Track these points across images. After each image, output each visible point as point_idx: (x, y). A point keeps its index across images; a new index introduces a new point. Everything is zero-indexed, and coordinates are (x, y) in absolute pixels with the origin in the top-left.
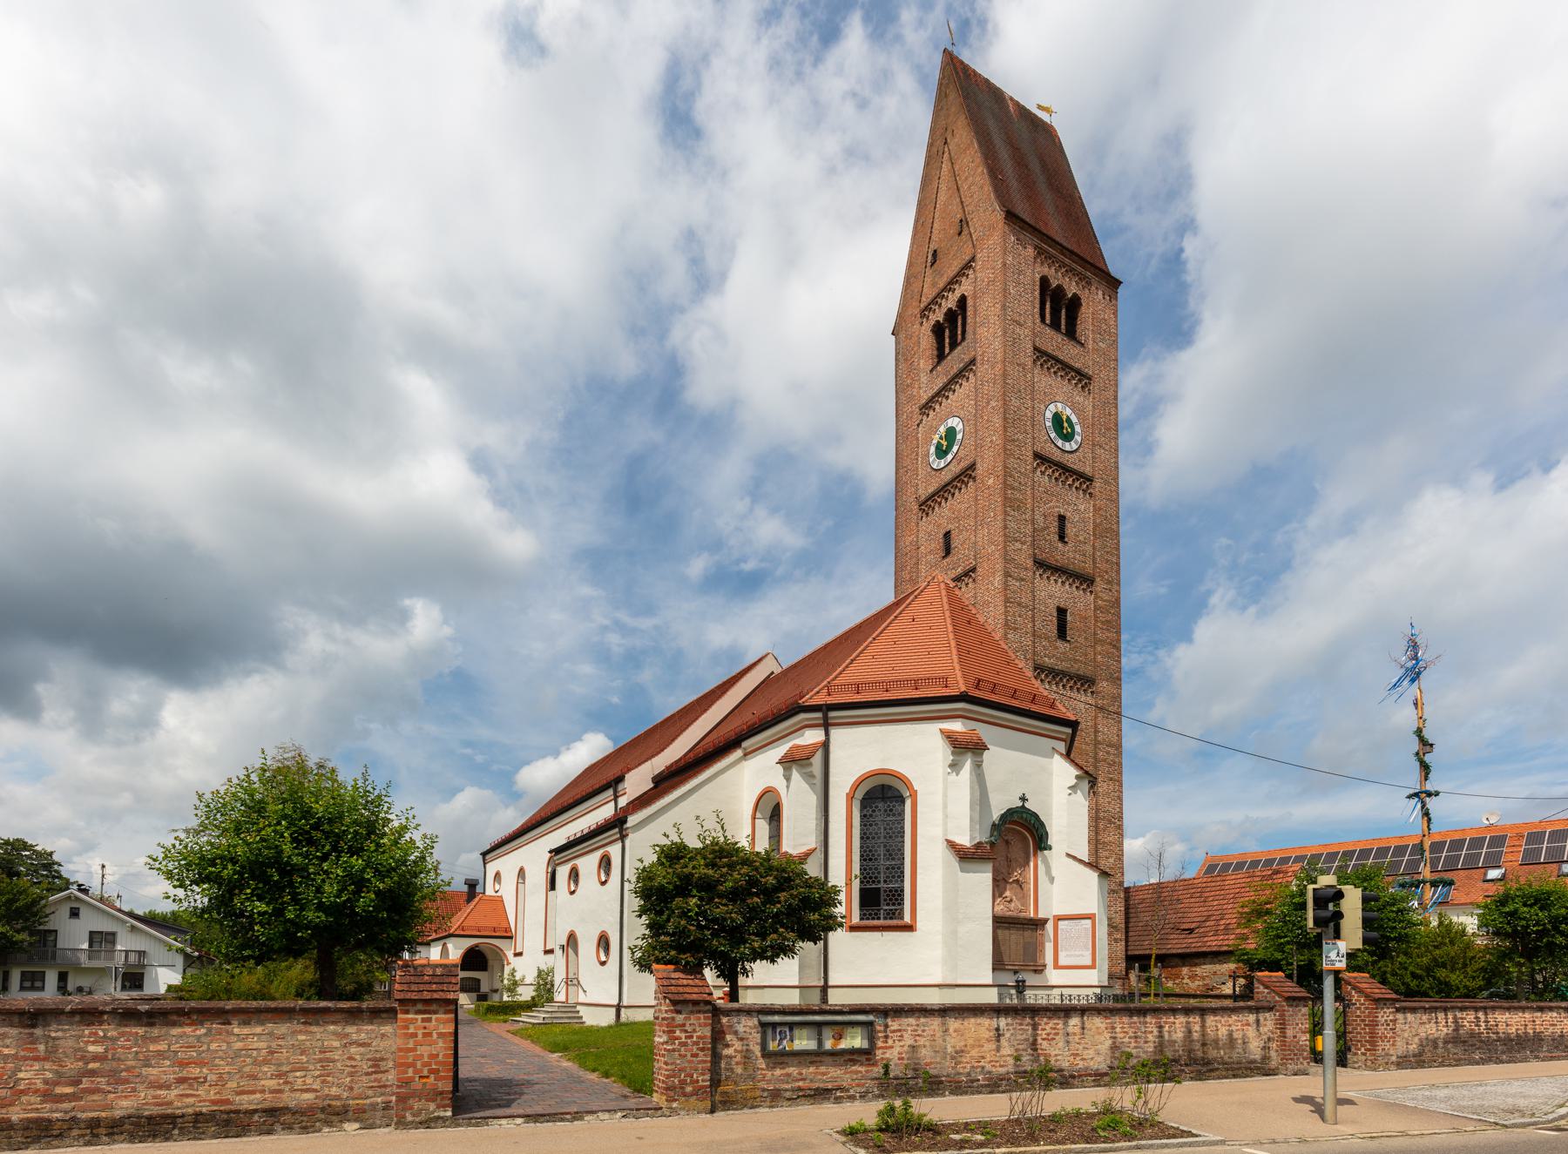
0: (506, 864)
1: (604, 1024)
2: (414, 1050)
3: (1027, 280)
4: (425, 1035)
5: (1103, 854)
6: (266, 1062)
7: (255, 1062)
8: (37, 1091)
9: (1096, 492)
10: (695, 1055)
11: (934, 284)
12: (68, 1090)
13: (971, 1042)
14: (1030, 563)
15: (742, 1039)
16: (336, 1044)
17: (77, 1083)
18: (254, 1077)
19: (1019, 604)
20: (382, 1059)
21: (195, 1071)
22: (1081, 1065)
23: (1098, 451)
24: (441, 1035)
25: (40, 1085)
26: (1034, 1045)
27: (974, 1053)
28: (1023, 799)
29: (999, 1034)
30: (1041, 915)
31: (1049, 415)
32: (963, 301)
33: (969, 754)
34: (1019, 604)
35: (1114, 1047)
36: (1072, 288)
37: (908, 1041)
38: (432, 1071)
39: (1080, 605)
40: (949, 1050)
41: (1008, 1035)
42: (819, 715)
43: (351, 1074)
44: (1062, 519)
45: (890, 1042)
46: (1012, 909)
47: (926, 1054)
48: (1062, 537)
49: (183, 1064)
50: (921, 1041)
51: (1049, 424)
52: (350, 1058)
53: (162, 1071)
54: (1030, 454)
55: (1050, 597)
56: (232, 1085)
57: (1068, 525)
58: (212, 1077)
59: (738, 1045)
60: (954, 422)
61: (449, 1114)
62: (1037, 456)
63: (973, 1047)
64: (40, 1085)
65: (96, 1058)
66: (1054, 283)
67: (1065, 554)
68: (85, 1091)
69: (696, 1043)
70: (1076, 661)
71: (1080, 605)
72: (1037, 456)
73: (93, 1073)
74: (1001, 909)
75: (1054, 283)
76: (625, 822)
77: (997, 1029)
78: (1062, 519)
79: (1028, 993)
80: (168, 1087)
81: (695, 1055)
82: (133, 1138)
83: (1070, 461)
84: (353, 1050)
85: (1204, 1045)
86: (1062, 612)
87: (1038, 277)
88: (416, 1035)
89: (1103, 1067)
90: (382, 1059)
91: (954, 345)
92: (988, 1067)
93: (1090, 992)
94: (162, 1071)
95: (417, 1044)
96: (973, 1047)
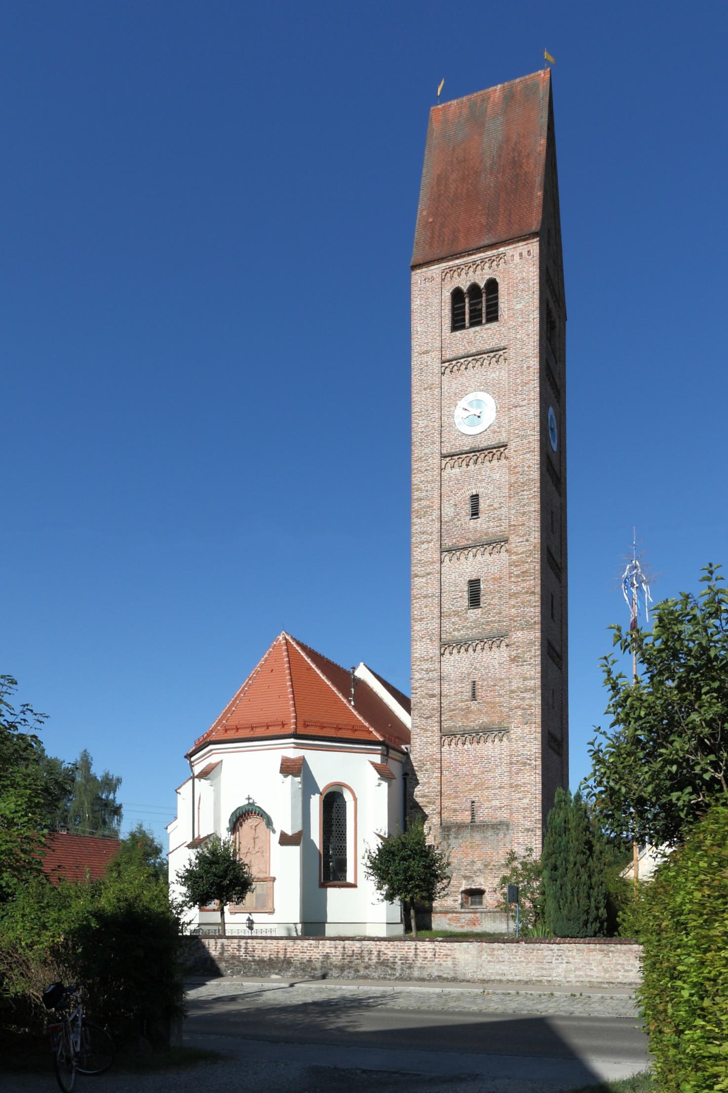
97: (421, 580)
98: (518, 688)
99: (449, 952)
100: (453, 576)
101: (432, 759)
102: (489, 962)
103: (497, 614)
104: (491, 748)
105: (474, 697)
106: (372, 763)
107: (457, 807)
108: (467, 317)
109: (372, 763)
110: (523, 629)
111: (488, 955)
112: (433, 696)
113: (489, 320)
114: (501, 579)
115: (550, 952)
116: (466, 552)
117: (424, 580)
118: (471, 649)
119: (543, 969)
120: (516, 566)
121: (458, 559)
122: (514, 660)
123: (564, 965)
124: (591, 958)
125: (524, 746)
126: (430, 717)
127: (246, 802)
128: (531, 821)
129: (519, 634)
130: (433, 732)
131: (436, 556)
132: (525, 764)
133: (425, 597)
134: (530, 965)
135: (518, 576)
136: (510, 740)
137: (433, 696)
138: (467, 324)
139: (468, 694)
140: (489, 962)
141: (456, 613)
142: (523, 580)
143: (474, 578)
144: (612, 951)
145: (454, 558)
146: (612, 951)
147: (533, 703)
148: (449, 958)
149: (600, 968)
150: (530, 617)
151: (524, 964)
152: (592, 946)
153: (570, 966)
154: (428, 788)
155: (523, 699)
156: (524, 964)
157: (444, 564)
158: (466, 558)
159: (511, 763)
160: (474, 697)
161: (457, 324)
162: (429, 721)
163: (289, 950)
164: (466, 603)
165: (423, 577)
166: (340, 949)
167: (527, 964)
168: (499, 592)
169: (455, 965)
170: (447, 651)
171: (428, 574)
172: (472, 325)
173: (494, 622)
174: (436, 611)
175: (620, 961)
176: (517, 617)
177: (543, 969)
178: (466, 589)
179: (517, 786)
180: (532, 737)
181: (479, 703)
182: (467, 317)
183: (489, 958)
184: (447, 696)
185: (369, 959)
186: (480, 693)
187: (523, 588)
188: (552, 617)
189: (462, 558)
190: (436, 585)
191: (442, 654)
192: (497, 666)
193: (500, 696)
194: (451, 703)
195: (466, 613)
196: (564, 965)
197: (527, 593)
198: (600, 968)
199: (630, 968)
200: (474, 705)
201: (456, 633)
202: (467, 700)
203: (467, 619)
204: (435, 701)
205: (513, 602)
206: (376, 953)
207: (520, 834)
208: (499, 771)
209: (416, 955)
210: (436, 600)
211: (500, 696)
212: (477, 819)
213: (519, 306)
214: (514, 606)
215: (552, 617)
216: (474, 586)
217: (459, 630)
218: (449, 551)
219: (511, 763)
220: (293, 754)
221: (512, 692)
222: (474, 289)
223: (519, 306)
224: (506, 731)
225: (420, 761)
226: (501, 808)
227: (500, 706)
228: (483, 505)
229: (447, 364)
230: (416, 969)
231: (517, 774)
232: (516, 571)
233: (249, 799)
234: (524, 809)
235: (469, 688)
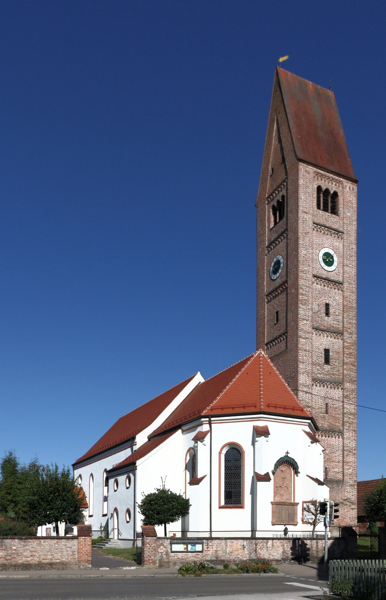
0: (84, 471)
1: (379, 477)
2: (82, 549)
3: (310, 190)
4: (85, 545)
5: (346, 467)
6: (49, 551)
7: (47, 552)
8: (3, 558)
9: (345, 289)
10: (152, 552)
11: (272, 185)
12: (9, 558)
13: (235, 549)
14: (310, 329)
15: (165, 547)
16: (64, 547)
17: (10, 556)
18: (46, 555)
19: (305, 350)
20: (74, 551)
21: (34, 553)
22: (272, 558)
23: (346, 268)
24: (88, 545)
25: (4, 556)
26: (256, 551)
27: (236, 553)
28: (287, 453)
29: (244, 547)
30: (296, 502)
31: (321, 255)
32: (283, 197)
33: (263, 437)
34: (305, 350)
35: (284, 552)
36: (333, 188)
37: (215, 549)
38: (86, 555)
39: (336, 347)
40: (228, 552)
41: (247, 547)
42: (208, 419)
43: (68, 555)
44: (327, 305)
45: (209, 549)
46: (284, 499)
47: (220, 553)
48: (327, 314)
49: (31, 552)
50: (219, 549)
51: (280, 271)
52: (67, 551)
53: (27, 553)
54: (311, 276)
55: (321, 345)
56: (42, 557)
57: (330, 308)
58: (37, 555)
59: (164, 549)
60: (280, 257)
61: (91, 566)
62: (343, 233)
63: (235, 551)
64: (4, 556)
65: (15, 550)
66: (324, 188)
67: (329, 321)
68: (13, 558)
69: (152, 548)
70: (333, 374)
71: (336, 347)
72: (314, 276)
73: (13, 553)
74: (278, 499)
75: (324, 188)
76: (135, 464)
77: (243, 545)
78: (327, 305)
79: (289, 533)
80: (29, 557)
81: (152, 552)
82: (22, 569)
83: (332, 277)
84: (68, 549)
85: (317, 552)
86: (327, 351)
87: (316, 186)
88: (82, 545)
89: (280, 558)
90: (74, 551)
91: (281, 218)
92: (240, 557)
93: (308, 533)
94: (27, 553)
95: (83, 547)
96: (235, 551)
105: (327, 412)
106: (304, 431)
109: (304, 431)
110: (349, 382)
117: (304, 341)
125: (350, 442)
129: (348, 384)
132: (350, 452)
135: (347, 354)
136: (343, 438)
139: (324, 410)
142: (350, 357)
147: (354, 421)
155: (349, 418)
160: (327, 412)
164: (323, 360)
165: (304, 339)
171: (307, 338)
181: (329, 416)
186: (330, 411)
187: (350, 361)
194: (316, 412)
197: (351, 364)
202: (324, 413)
207: (348, 487)
217: (320, 374)
226: (338, 473)
231: (347, 456)
234: (350, 474)
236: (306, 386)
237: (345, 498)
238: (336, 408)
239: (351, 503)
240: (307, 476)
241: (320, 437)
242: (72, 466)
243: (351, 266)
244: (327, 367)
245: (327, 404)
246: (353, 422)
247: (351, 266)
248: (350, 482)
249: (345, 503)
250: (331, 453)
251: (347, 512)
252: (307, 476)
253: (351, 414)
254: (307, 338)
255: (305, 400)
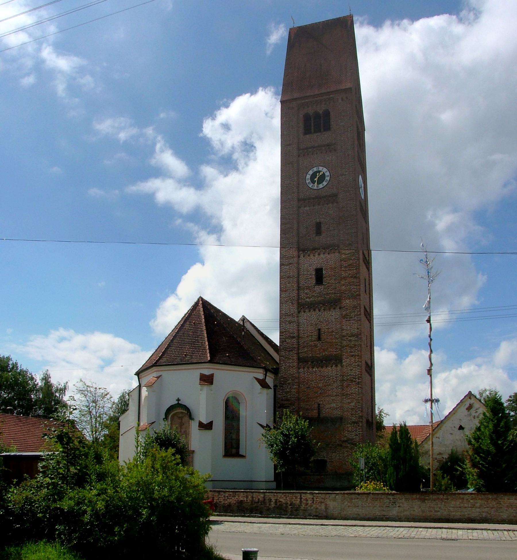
97: (286, 267)
98: (347, 334)
99: (323, 500)
100: (305, 266)
101: (293, 377)
102: (349, 506)
103: (334, 289)
104: (331, 371)
105: (319, 338)
106: (256, 379)
107: (308, 407)
108: (312, 128)
109: (256, 379)
110: (349, 299)
111: (349, 502)
112: (294, 337)
113: (325, 130)
114: (335, 268)
115: (388, 500)
116: (314, 252)
117: (288, 267)
118: (317, 310)
119: (384, 511)
120: (345, 261)
121: (309, 256)
122: (344, 317)
123: (397, 508)
124: (414, 504)
125: (351, 370)
126: (292, 351)
127: (177, 402)
128: (356, 417)
129: (347, 301)
130: (293, 360)
131: (295, 254)
132: (352, 381)
133: (288, 278)
134: (375, 508)
135: (345, 267)
136: (342, 366)
137: (294, 337)
138: (312, 130)
139: (315, 337)
140: (349, 506)
141: (308, 288)
142: (349, 270)
143: (319, 267)
144: (427, 499)
145: (307, 256)
146: (427, 499)
147: (356, 343)
148: (323, 504)
149: (420, 510)
150: (354, 291)
151: (371, 508)
152: (414, 496)
153: (401, 509)
154: (290, 395)
155: (350, 341)
156: (371, 508)
157: (300, 258)
158: (314, 256)
159: (343, 380)
160: (319, 338)
161: (307, 131)
162: (291, 353)
163: (216, 498)
164: (314, 282)
165: (287, 265)
166: (250, 498)
167: (374, 507)
168: (334, 276)
169: (326, 508)
170: (302, 311)
171: (290, 264)
172: (315, 132)
173: (332, 294)
174: (295, 286)
175: (432, 505)
176: (346, 291)
177: (384, 511)
178: (314, 273)
179: (347, 394)
180: (356, 364)
181: (323, 343)
182: (312, 128)
183: (349, 504)
184: (302, 338)
185: (269, 505)
186: (323, 336)
187: (349, 274)
188: (366, 291)
189: (312, 255)
190: (295, 271)
191: (299, 312)
192: (334, 320)
193: (336, 338)
194: (304, 342)
195: (314, 288)
196: (397, 508)
197: (352, 277)
198: (420, 510)
199: (438, 509)
200: (318, 344)
201: (308, 300)
202: (315, 341)
203: (315, 291)
204: (295, 341)
205: (343, 282)
206: (274, 501)
207: (349, 425)
208: (335, 385)
209: (301, 502)
210: (295, 280)
211: (336, 338)
212: (321, 416)
213: (342, 124)
214: (344, 285)
215: (366, 291)
216: (319, 272)
217: (309, 298)
218: (303, 251)
219: (343, 380)
220: (207, 372)
221: (344, 336)
222: (317, 115)
223: (342, 124)
224: (341, 361)
225: (285, 378)
226: (337, 408)
227: (336, 345)
228: (323, 228)
229: (301, 151)
230: (300, 511)
231: (347, 387)
232: (344, 264)
233: (178, 400)
234: (351, 409)
235: (316, 333)
236: (290, 315)
237: (345, 439)
238: (333, 332)
239: (353, 444)
240: (259, 424)
241: (204, 405)
242: (136, 377)
243: (347, 173)
244: (318, 289)
245: (319, 330)
246: (355, 345)
247: (347, 173)
248: (351, 419)
249: (344, 445)
250: (325, 386)
251: (348, 456)
252: (259, 424)
253: (353, 336)
254: (290, 264)
255: (289, 331)
